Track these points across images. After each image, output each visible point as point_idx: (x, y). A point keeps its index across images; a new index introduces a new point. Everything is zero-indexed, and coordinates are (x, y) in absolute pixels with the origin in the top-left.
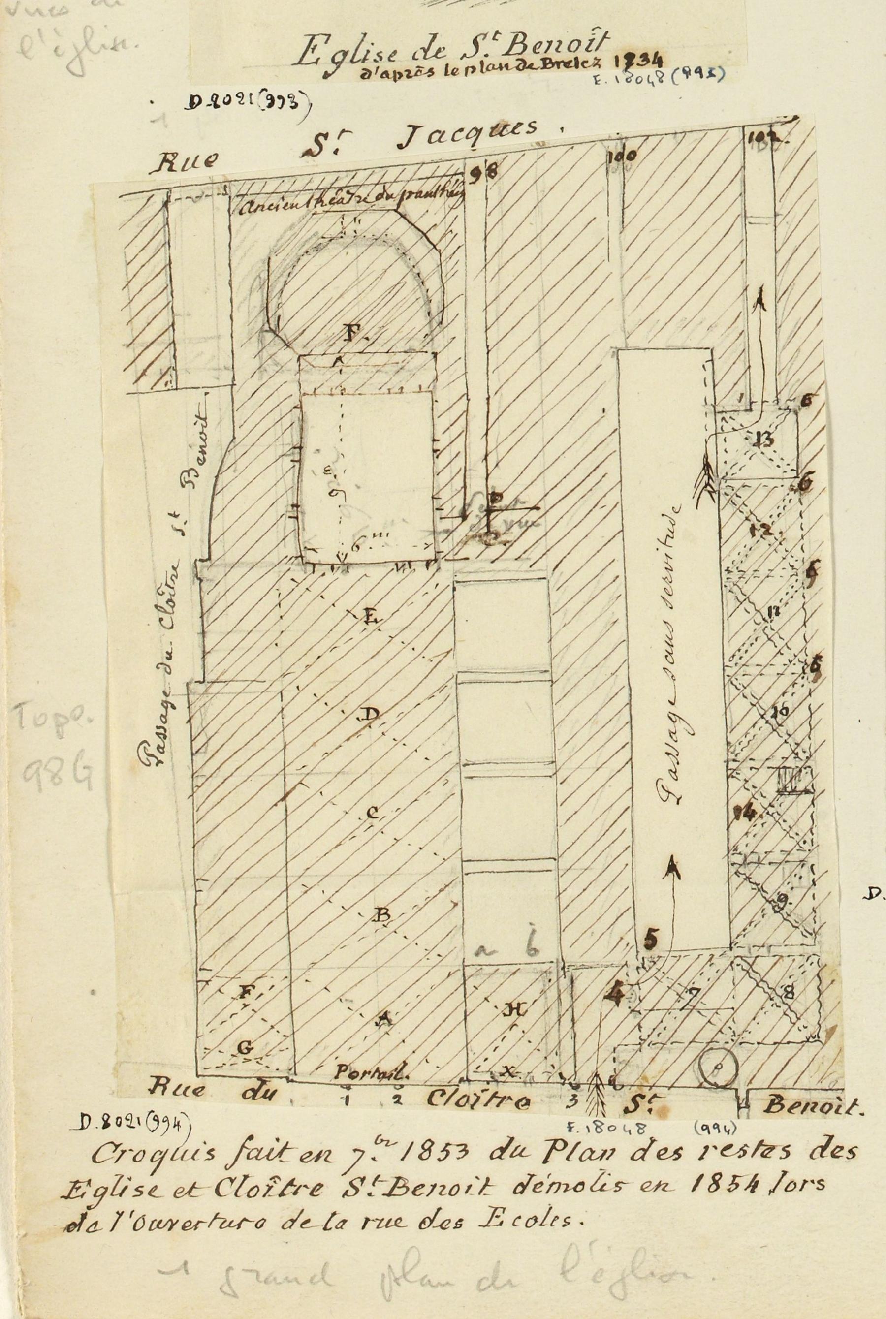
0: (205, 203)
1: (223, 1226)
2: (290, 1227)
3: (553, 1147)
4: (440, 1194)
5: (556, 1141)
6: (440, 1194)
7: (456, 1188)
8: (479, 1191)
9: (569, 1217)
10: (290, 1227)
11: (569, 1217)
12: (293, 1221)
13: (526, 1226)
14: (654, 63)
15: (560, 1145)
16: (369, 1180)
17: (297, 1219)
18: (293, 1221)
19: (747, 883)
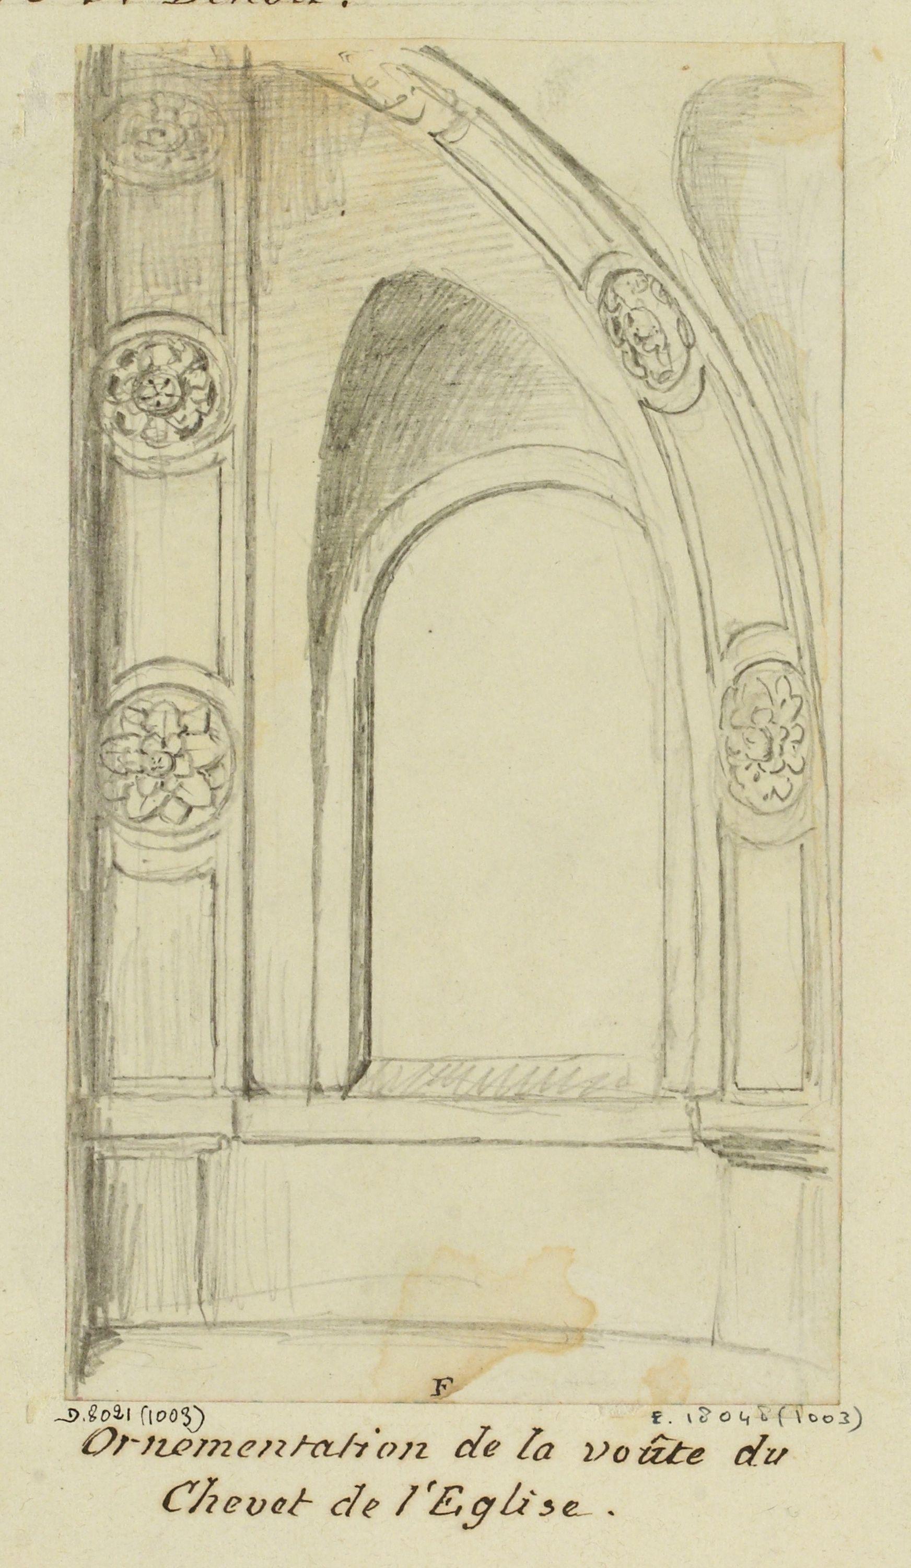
6: (157, 1454)
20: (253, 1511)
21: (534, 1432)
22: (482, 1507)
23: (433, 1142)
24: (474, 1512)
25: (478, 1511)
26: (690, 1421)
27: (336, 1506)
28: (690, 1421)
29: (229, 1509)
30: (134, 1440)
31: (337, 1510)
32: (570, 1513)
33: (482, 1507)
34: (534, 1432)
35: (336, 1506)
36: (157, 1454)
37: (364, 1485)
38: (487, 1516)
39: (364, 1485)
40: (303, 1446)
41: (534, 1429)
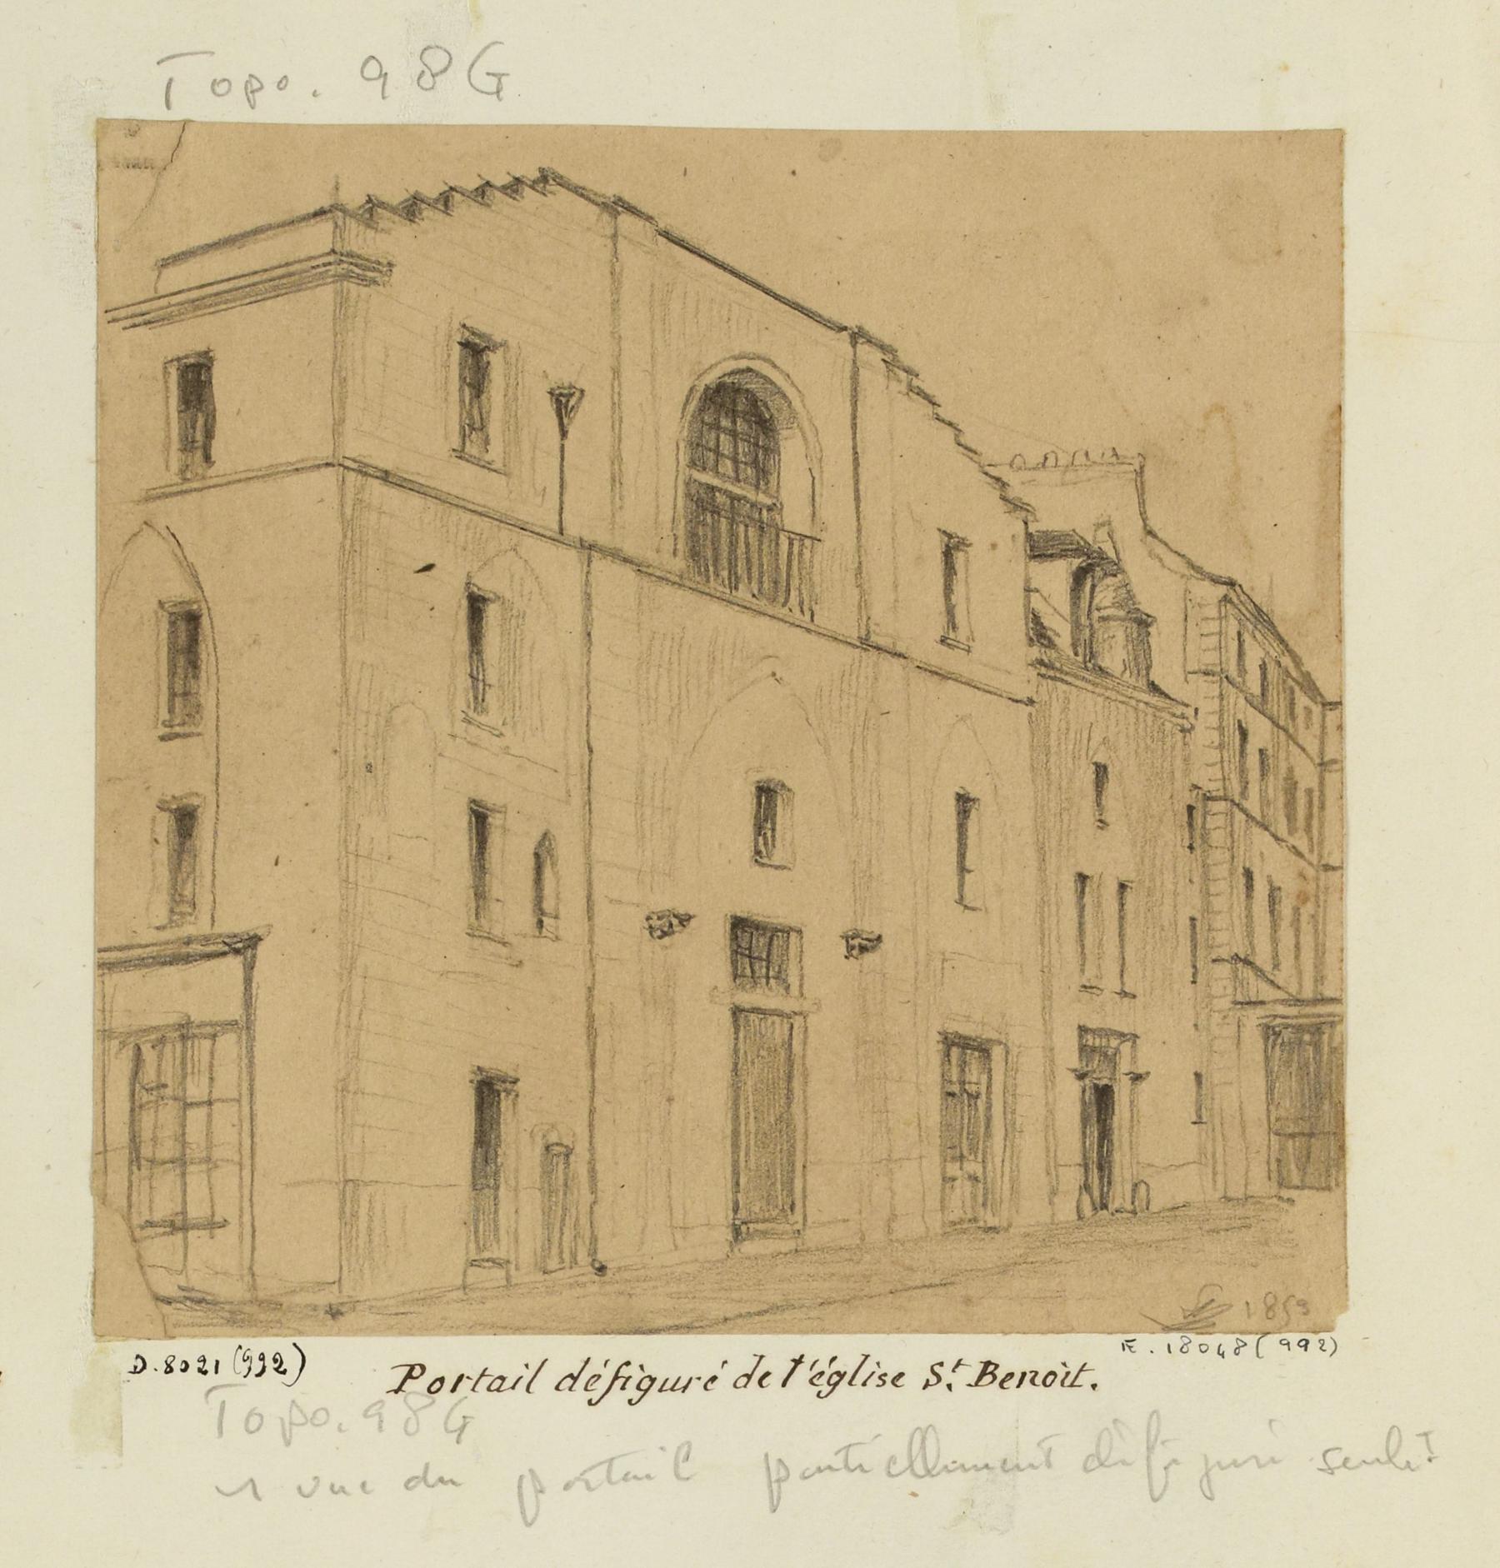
0: (945, 1460)
1: (530, 1515)
2: (745, 1386)
3: (409, 1376)
4: (1036, 1373)
5: (412, 1368)
6: (1036, 1373)
7: (433, 1389)
8: (227, 1406)
9: (878, 1386)
10: (745, 1386)
11: (878, 1386)
12: (749, 1377)
13: (407, 1433)
14: (1102, 1209)
15: (417, 1372)
16: (949, 1365)
17: (753, 1373)
18: (749, 1377)
19: (158, 1170)
20: (1048, 1383)
21: (793, 1364)
22: (835, 1378)
23: (756, 1367)
24: (638, 1388)
25: (832, 1382)
26: (1170, 1352)
27: (560, 1383)
28: (1170, 1352)
29: (589, 1388)
30: (468, 1378)
31: (738, 1385)
32: (934, 1472)
33: (835, 1378)
34: (793, 1364)
35: (560, 1383)
36: (1036, 1373)
37: (630, 1377)
38: (837, 1388)
39: (630, 1377)
40: (483, 1378)
41: (794, 1360)
